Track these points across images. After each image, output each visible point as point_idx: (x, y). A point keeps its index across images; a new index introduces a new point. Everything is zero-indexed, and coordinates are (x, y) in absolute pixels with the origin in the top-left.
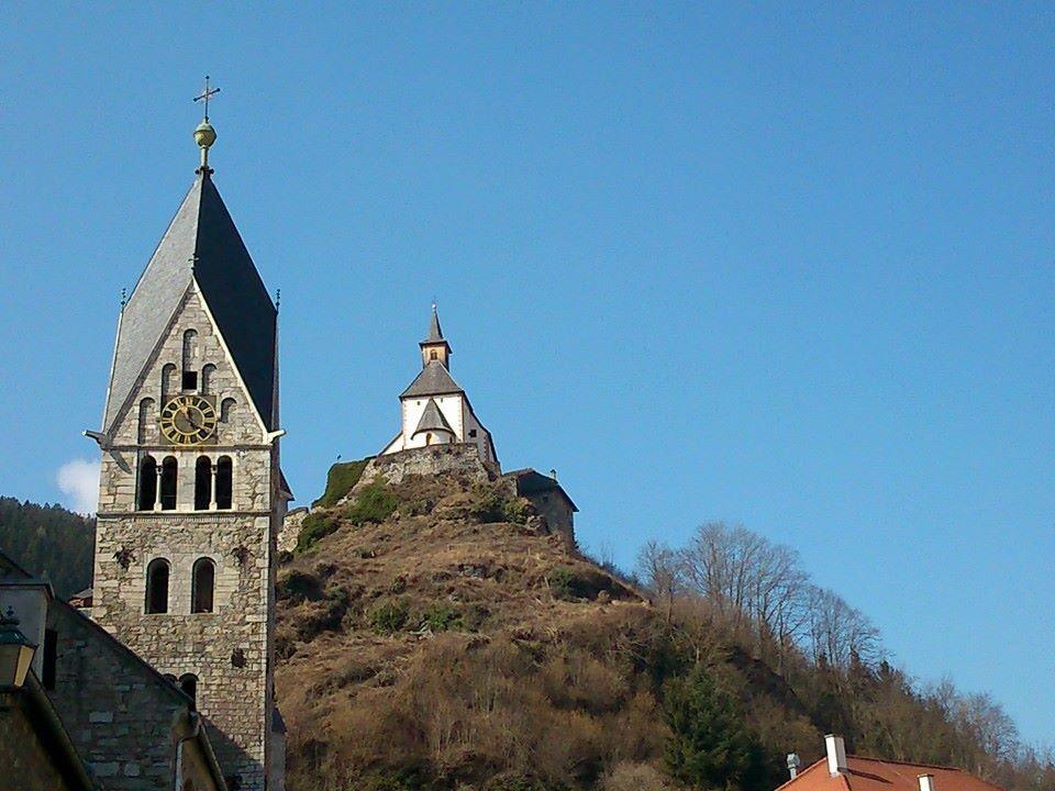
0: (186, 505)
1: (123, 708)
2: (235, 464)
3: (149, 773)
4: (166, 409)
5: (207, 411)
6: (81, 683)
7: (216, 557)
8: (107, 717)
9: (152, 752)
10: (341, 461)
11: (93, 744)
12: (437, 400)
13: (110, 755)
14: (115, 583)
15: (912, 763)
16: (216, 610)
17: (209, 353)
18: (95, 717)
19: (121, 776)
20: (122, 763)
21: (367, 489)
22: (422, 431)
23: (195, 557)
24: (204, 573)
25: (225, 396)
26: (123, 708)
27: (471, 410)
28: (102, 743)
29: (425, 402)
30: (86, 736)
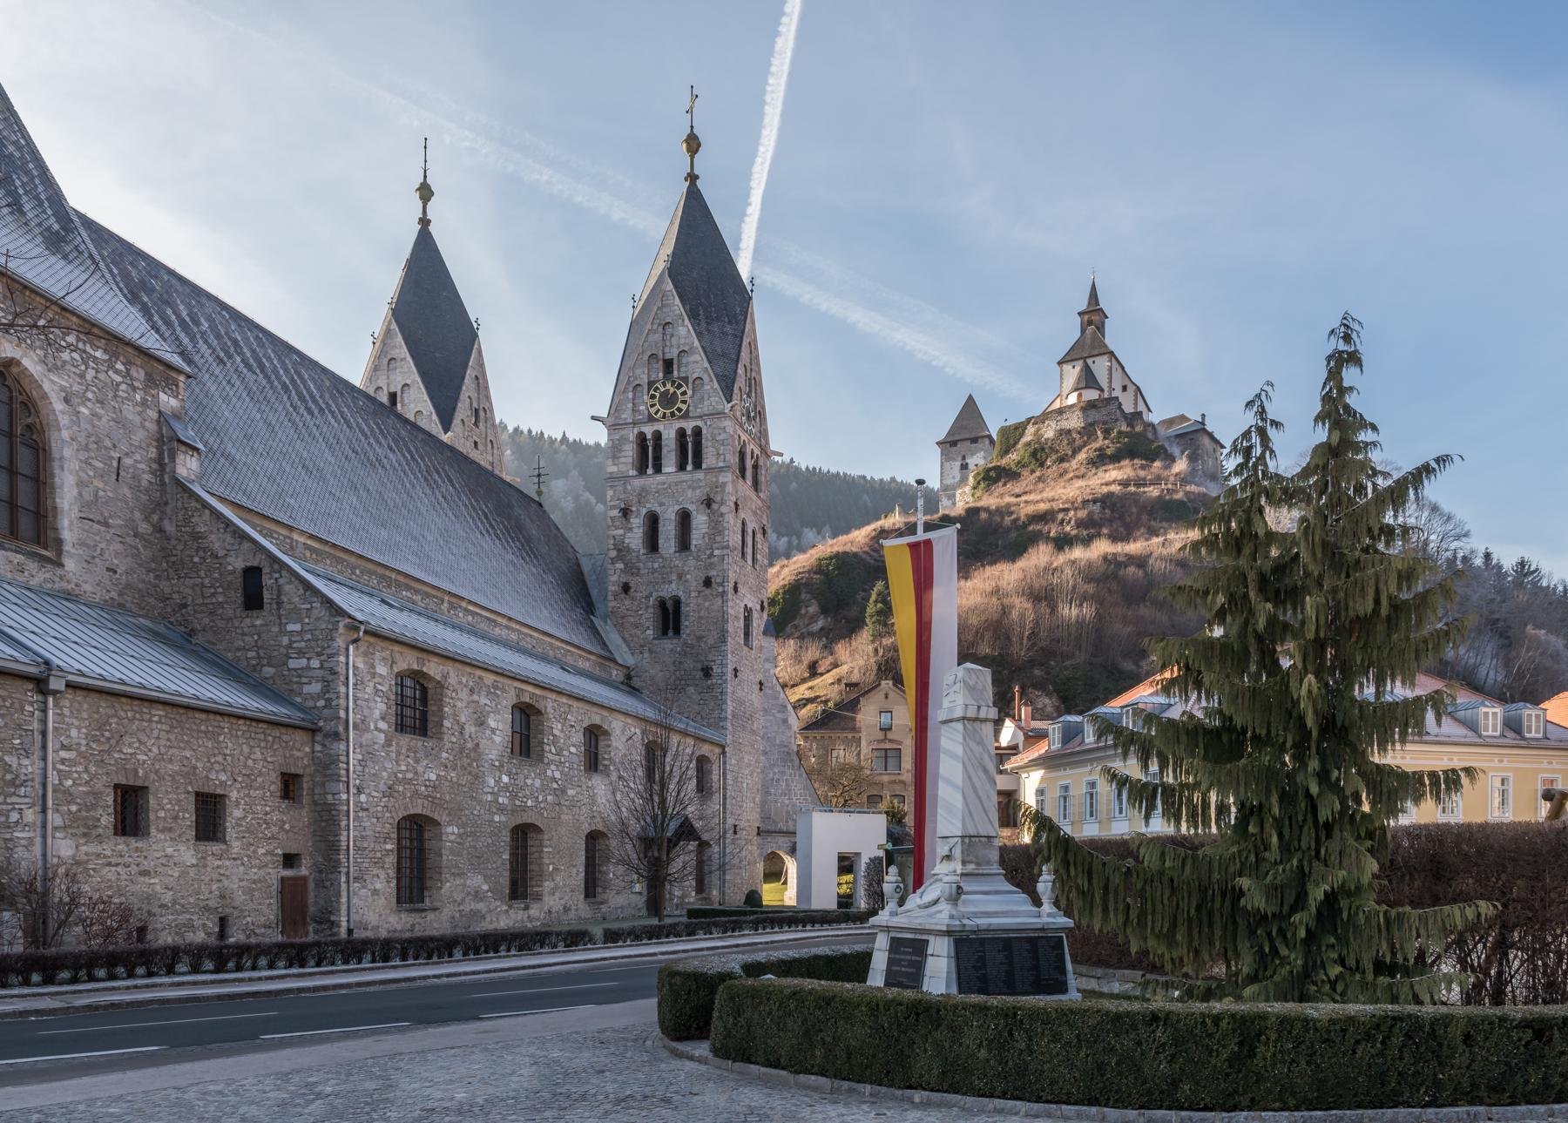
0: (669, 467)
1: (307, 620)
2: (704, 432)
3: (326, 665)
4: (652, 392)
5: (682, 390)
6: (280, 603)
7: (692, 508)
8: (297, 627)
9: (328, 651)
10: (1008, 424)
11: (289, 646)
12: (1090, 361)
13: (301, 653)
14: (621, 532)
15: (439, 617)
16: (693, 548)
17: (682, 341)
18: (290, 627)
19: (308, 668)
20: (309, 659)
21: (1028, 444)
22: (1076, 390)
23: (677, 508)
24: (685, 518)
25: (695, 376)
26: (307, 620)
27: (1123, 368)
28: (295, 645)
29: (1081, 362)
30: (285, 641)
